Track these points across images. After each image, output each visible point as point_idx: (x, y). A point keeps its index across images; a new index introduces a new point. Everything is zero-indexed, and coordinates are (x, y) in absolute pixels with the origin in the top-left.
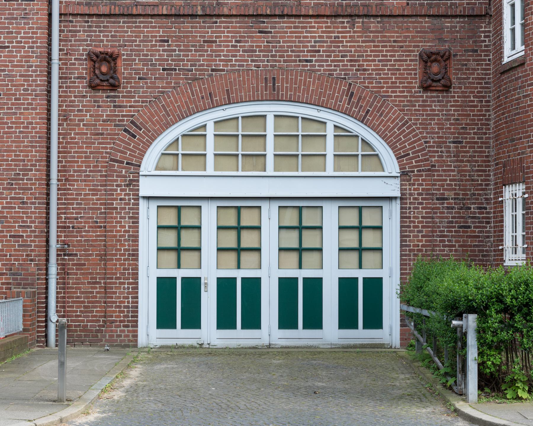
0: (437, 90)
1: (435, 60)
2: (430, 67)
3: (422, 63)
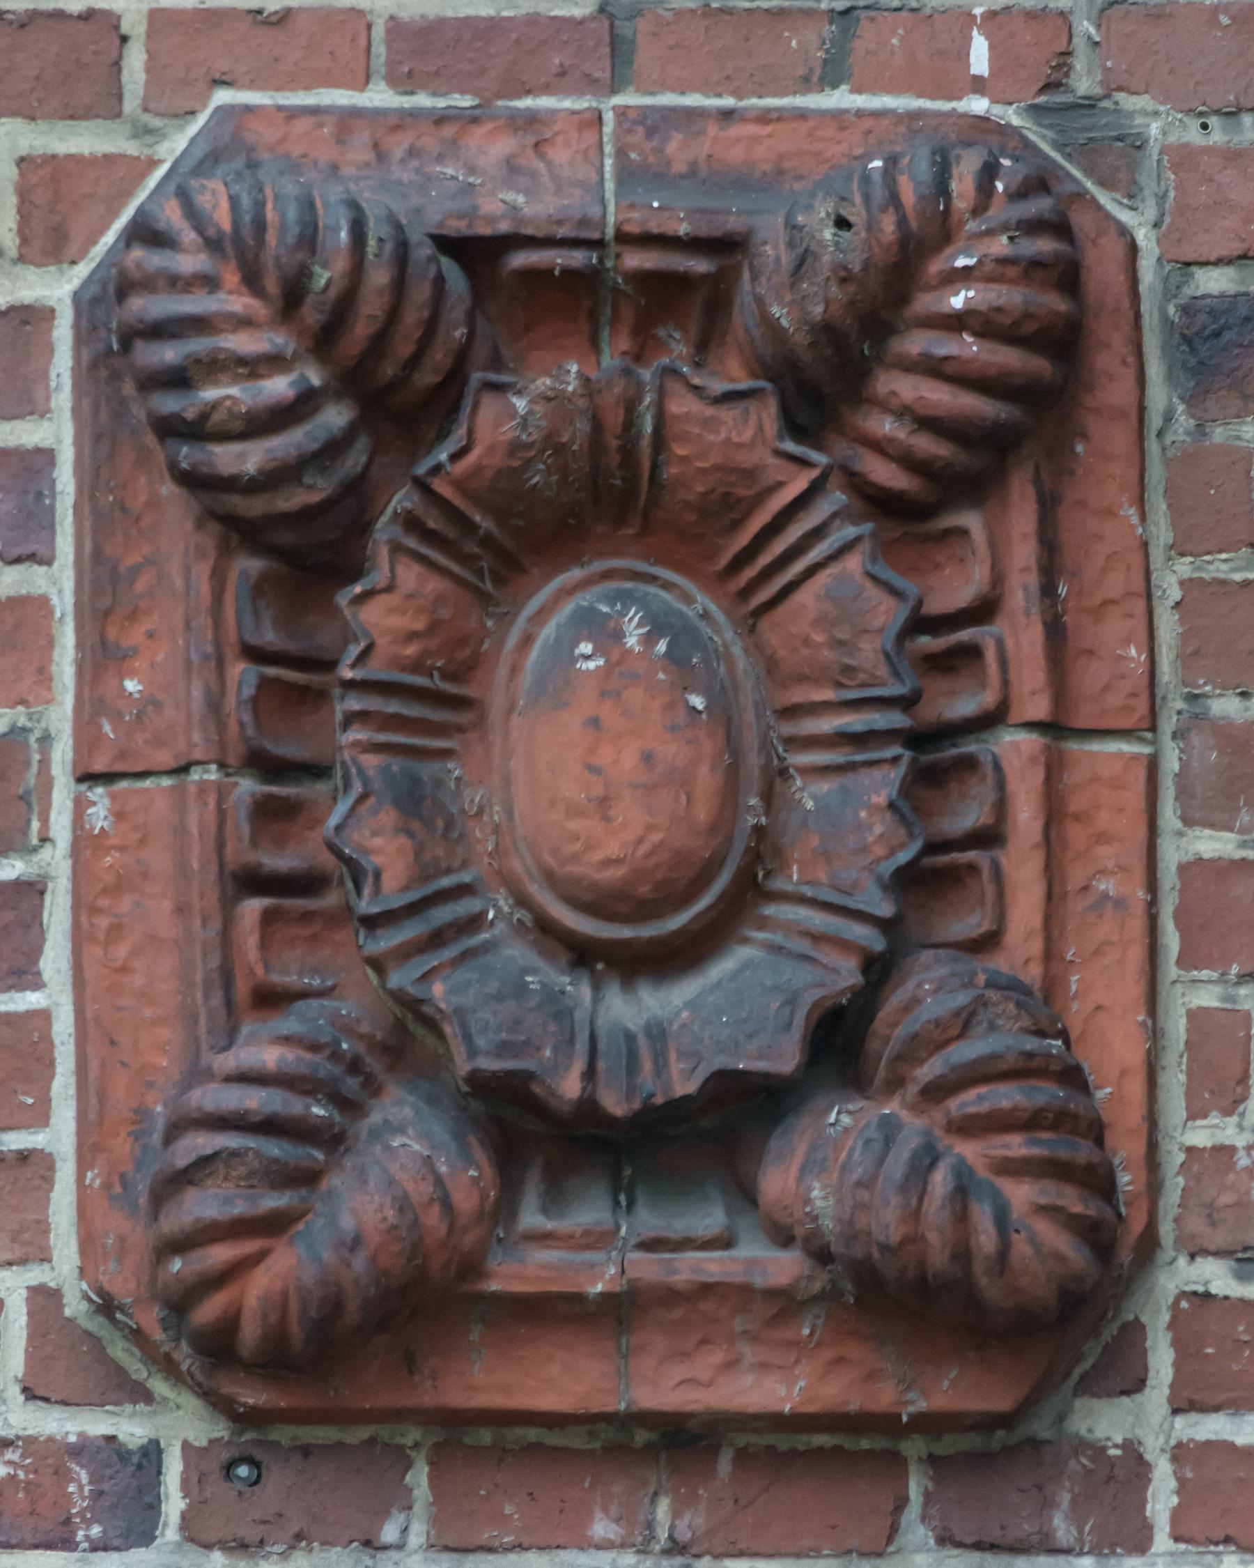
0: (681, 1442)
1: (602, 501)
2: (442, 698)
3: (175, 544)
